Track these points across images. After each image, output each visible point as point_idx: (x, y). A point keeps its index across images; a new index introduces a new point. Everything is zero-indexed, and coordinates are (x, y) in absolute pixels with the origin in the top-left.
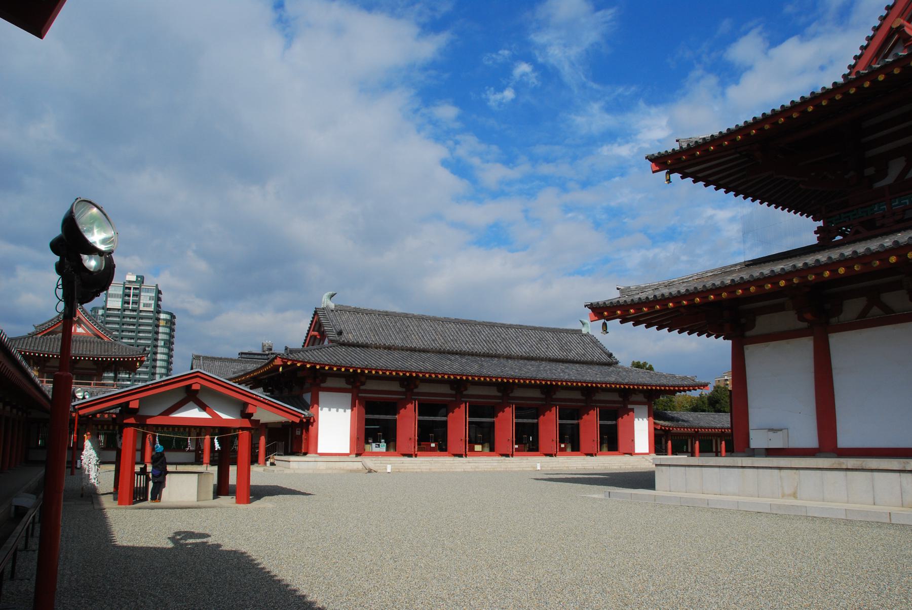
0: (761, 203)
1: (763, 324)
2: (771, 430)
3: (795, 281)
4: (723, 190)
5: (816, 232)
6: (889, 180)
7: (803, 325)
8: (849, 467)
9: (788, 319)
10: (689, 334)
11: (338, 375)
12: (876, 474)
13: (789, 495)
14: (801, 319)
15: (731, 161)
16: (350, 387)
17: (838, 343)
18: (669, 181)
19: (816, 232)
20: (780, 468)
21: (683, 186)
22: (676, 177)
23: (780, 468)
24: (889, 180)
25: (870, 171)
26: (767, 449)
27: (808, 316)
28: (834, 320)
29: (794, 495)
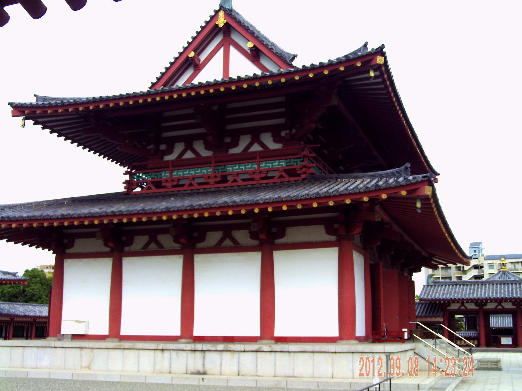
0: (94, 153)
1: (79, 245)
2: (77, 321)
3: (14, 226)
4: (70, 141)
5: (124, 183)
6: (172, 157)
7: (107, 249)
8: (126, 347)
9: (97, 245)
10: (30, 246)
11: (232, 17)
12: (141, 351)
13: (86, 367)
14: (106, 245)
15: (67, 119)
16: (333, 238)
17: (127, 263)
18: (24, 125)
19: (124, 183)
20: (81, 348)
21: (34, 130)
22: (30, 122)
23: (81, 348)
24: (172, 157)
25: (163, 147)
26: (73, 335)
27: (111, 244)
28: (127, 249)
29: (89, 367)
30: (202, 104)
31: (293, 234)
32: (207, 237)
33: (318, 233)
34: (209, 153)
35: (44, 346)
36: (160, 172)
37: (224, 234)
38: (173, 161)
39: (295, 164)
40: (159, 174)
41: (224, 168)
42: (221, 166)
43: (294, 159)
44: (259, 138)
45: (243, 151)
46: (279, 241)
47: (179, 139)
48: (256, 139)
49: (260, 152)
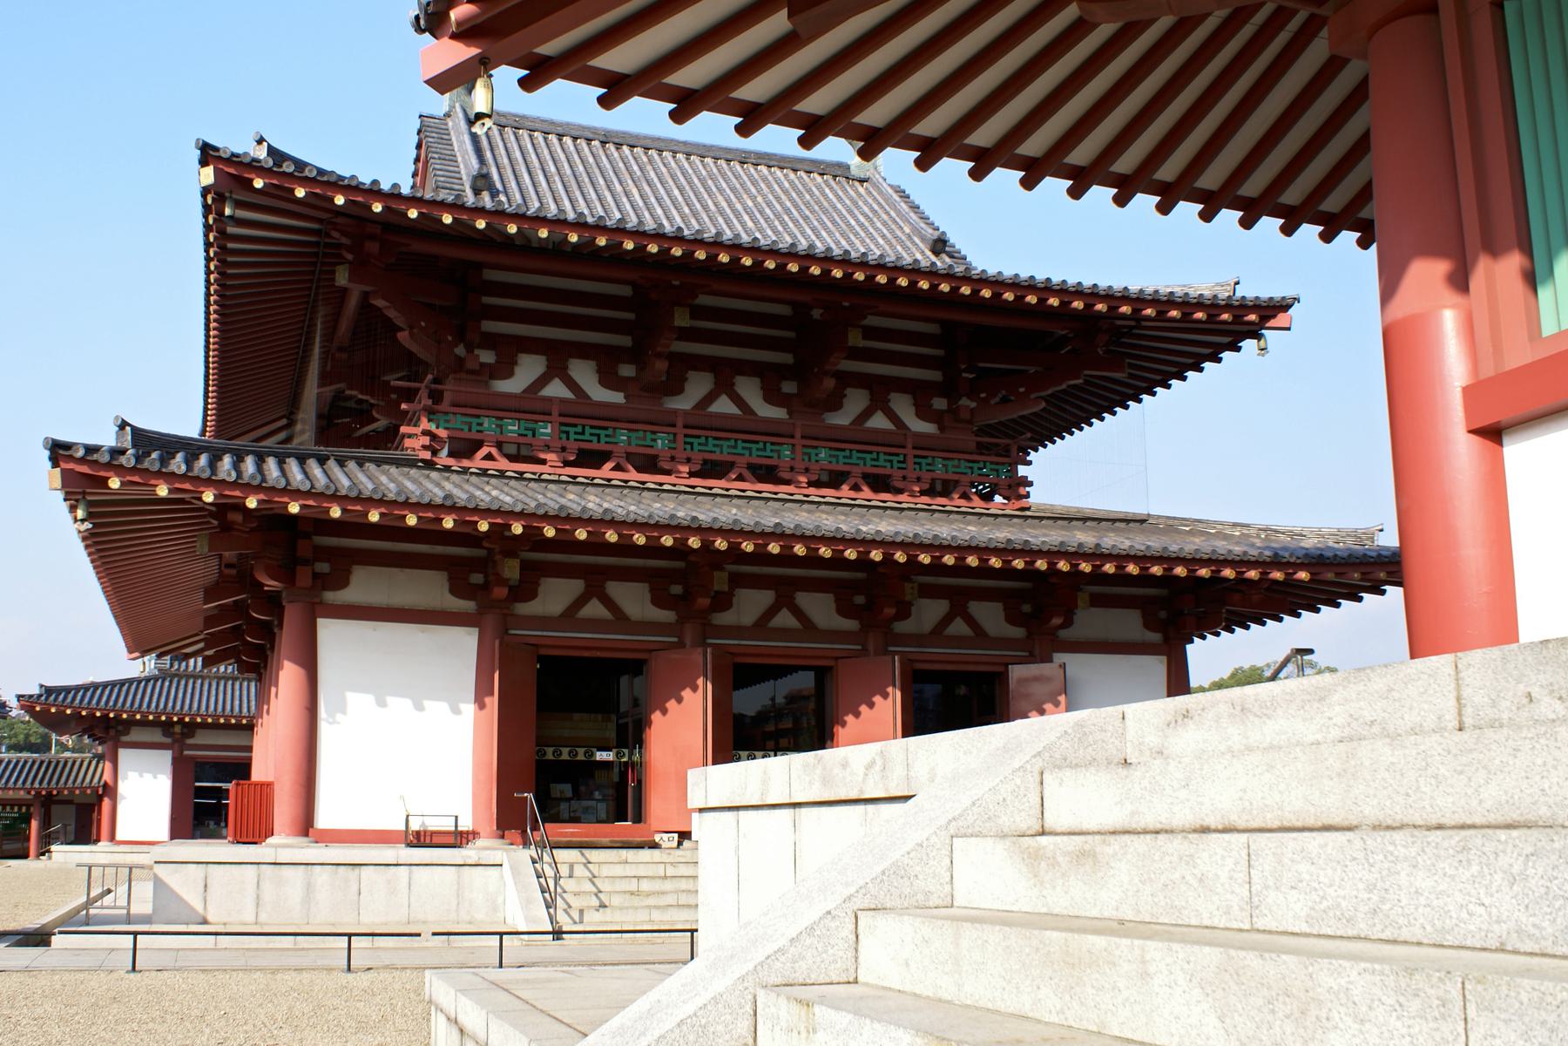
1: (136, 735)
30: (676, 283)
31: (364, 586)
32: (541, 589)
33: (431, 589)
34: (778, 413)
35: (1150, 821)
36: (478, 416)
37: (952, 606)
38: (686, 413)
39: (466, 428)
40: (475, 421)
41: (613, 436)
42: (606, 428)
43: (716, 438)
44: (566, 368)
45: (854, 422)
46: (331, 597)
47: (863, 381)
48: (556, 369)
49: (563, 401)
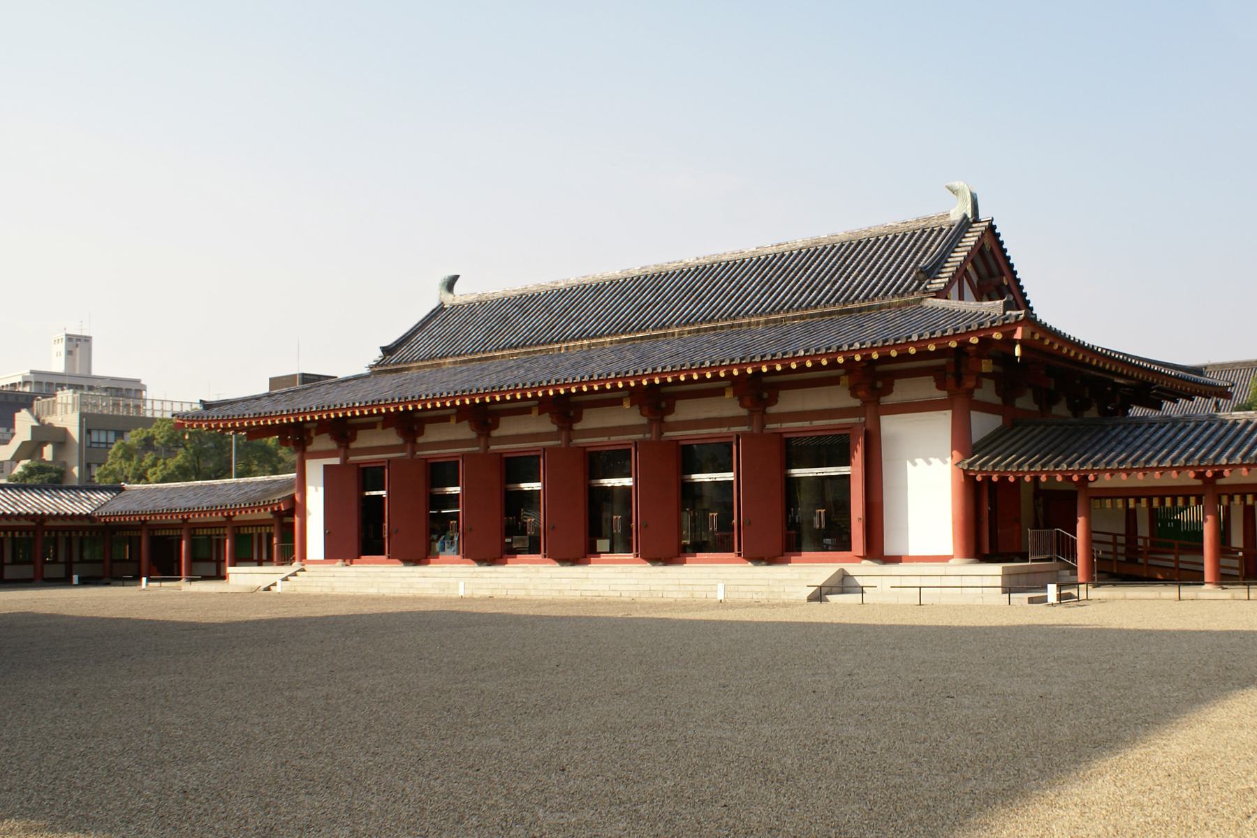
1: (903, 391)
7: (942, 395)
